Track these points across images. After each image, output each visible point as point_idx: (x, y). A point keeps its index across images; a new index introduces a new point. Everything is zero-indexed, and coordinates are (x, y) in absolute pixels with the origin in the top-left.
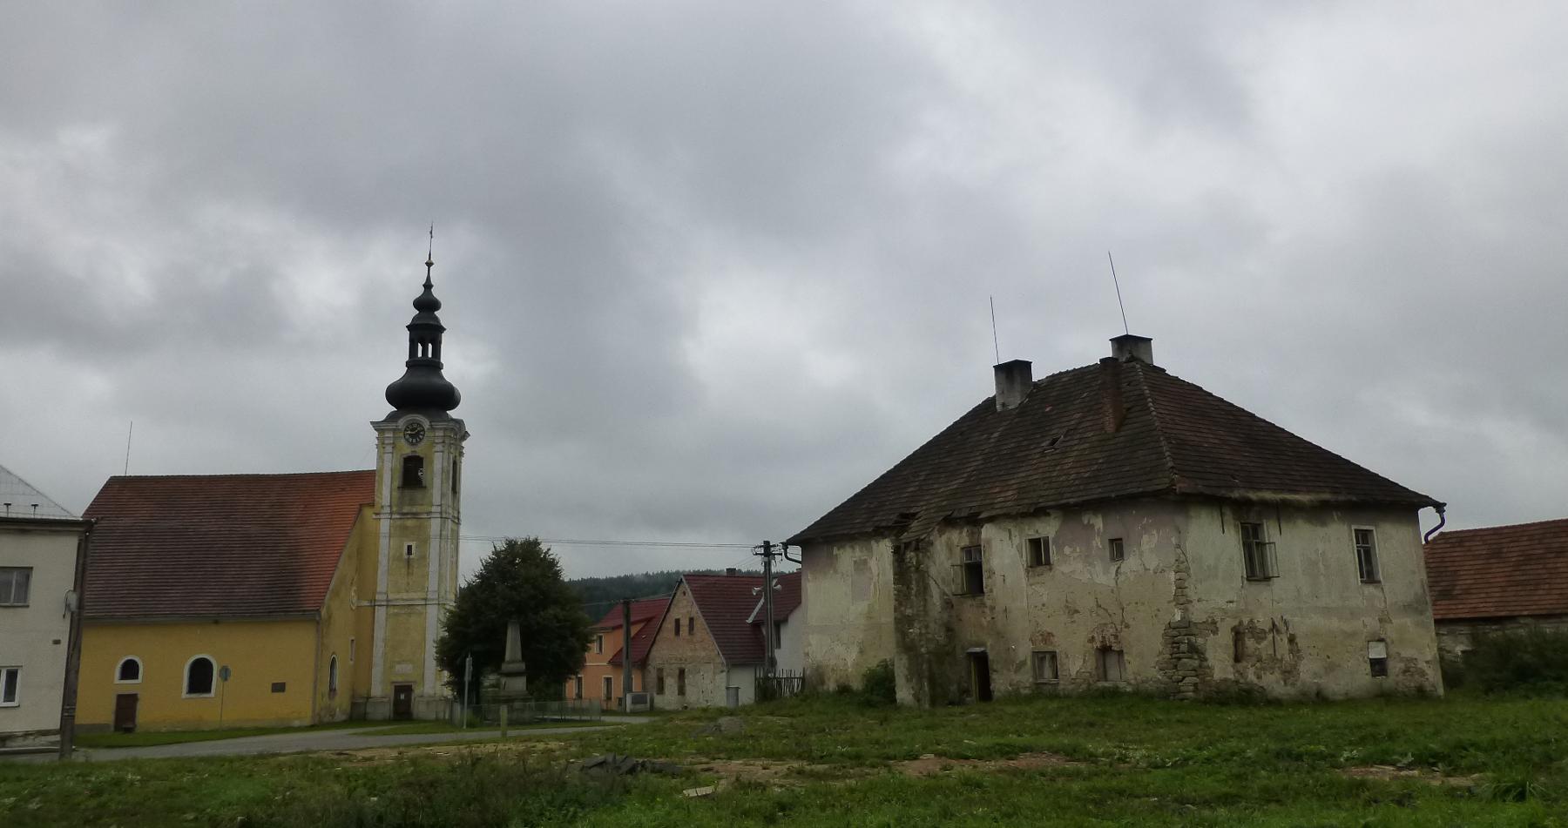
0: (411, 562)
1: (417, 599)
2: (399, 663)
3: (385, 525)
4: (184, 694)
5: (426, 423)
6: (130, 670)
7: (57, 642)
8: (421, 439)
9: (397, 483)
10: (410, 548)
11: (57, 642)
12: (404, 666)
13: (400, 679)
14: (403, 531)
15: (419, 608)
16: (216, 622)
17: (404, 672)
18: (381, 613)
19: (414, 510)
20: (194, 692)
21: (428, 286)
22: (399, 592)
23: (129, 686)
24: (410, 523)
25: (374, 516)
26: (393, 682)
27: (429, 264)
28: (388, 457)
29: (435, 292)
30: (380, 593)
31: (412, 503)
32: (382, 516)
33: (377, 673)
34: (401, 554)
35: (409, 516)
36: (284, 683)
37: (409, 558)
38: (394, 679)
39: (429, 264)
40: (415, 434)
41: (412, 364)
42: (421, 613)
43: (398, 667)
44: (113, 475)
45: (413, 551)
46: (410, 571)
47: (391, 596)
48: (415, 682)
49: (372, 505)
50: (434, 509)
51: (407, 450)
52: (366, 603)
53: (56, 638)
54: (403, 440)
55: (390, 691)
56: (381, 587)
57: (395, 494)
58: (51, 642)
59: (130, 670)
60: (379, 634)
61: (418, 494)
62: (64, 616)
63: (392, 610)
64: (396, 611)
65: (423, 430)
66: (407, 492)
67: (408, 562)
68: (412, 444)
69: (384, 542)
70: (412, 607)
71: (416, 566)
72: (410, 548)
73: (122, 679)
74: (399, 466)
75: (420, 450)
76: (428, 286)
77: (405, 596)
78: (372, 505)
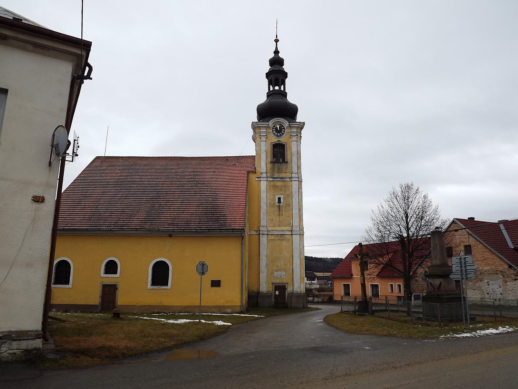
0: (281, 207)
1: (287, 230)
2: (276, 271)
3: (264, 185)
4: (149, 286)
5: (286, 123)
6: (111, 267)
7: (38, 200)
8: (283, 134)
9: (269, 160)
10: (279, 199)
11: (38, 200)
12: (280, 273)
13: (278, 281)
14: (273, 188)
15: (288, 236)
16: (170, 236)
17: (280, 277)
18: (264, 239)
19: (281, 176)
20: (284, 285)
21: (276, 52)
22: (274, 226)
23: (110, 279)
24: (279, 184)
25: (257, 180)
26: (273, 284)
27: (277, 41)
28: (263, 144)
29: (281, 55)
30: (263, 226)
31: (280, 171)
32: (262, 179)
33: (263, 276)
34: (275, 204)
35: (278, 180)
36: (220, 281)
37: (279, 206)
38: (274, 282)
39: (277, 41)
40: (279, 131)
41: (270, 95)
42: (289, 240)
43: (276, 273)
44: (102, 154)
45: (282, 200)
46: (281, 213)
47: (269, 229)
48: (287, 283)
49: (254, 172)
50: (294, 175)
51: (275, 140)
52: (254, 233)
53: (39, 194)
54: (272, 134)
55: (271, 289)
56: (263, 223)
57: (269, 166)
58: (30, 198)
59: (111, 267)
60: (264, 252)
61: (284, 166)
62: (50, 164)
63: (270, 237)
64: (273, 238)
65: (284, 128)
66: (276, 165)
67: (279, 208)
68: (277, 136)
69: (263, 195)
70: (284, 235)
71: (283, 210)
72: (279, 199)
73: (105, 274)
74: (270, 148)
75: (283, 139)
76: (276, 52)
77: (278, 228)
78: (254, 172)
